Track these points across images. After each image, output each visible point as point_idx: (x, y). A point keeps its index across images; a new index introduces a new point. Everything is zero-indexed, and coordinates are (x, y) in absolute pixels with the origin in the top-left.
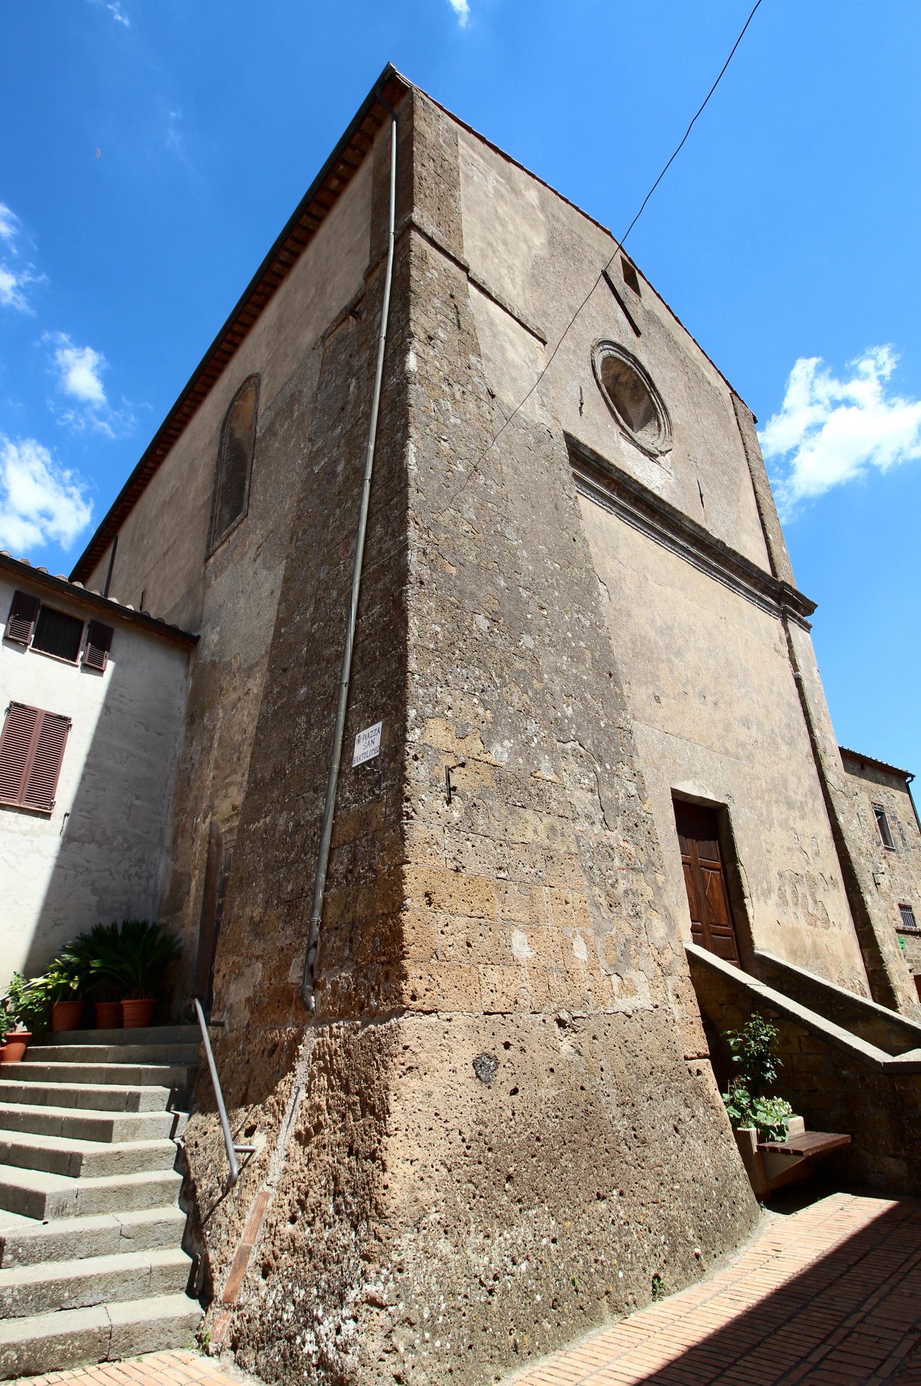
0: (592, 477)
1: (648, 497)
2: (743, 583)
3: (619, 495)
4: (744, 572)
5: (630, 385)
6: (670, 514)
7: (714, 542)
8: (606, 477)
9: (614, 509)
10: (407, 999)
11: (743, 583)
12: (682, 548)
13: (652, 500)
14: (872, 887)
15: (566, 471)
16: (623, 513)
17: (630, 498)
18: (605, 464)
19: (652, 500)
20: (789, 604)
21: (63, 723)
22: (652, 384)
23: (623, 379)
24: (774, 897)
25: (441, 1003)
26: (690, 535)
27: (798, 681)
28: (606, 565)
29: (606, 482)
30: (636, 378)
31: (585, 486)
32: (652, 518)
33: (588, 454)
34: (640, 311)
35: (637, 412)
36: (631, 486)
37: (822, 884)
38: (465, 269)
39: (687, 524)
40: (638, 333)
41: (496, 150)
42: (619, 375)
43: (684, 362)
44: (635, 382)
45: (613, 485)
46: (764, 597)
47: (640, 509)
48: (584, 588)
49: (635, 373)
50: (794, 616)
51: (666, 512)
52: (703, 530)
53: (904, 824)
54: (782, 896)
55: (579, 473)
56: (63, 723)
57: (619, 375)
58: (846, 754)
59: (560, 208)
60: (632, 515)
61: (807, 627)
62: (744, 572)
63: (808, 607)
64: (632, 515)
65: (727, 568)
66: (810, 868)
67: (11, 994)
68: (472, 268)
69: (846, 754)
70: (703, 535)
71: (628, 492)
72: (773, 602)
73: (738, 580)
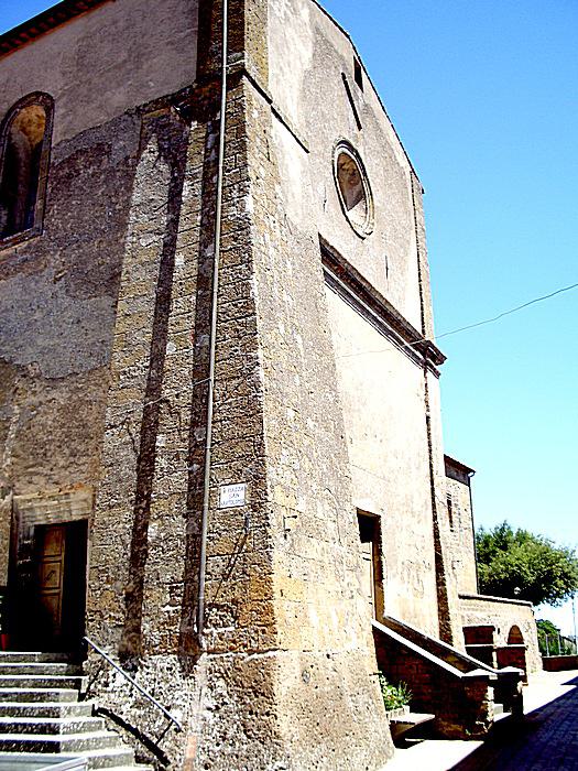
5: (351, 172)
7: (457, 665)
10: (277, 643)
14: (450, 571)
15: (318, 266)
20: (428, 356)
21: (75, 534)
22: (365, 174)
24: (399, 576)
25: (289, 647)
27: (431, 466)
28: (348, 379)
34: (361, 102)
35: (352, 194)
37: (423, 568)
38: (270, 101)
40: (360, 127)
43: (386, 146)
48: (328, 373)
50: (431, 366)
53: (462, 511)
54: (402, 579)
55: (326, 269)
56: (75, 534)
58: (447, 459)
59: (327, 23)
61: (437, 375)
63: (439, 358)
66: (418, 558)
68: (274, 98)
69: (447, 459)
72: (421, 357)
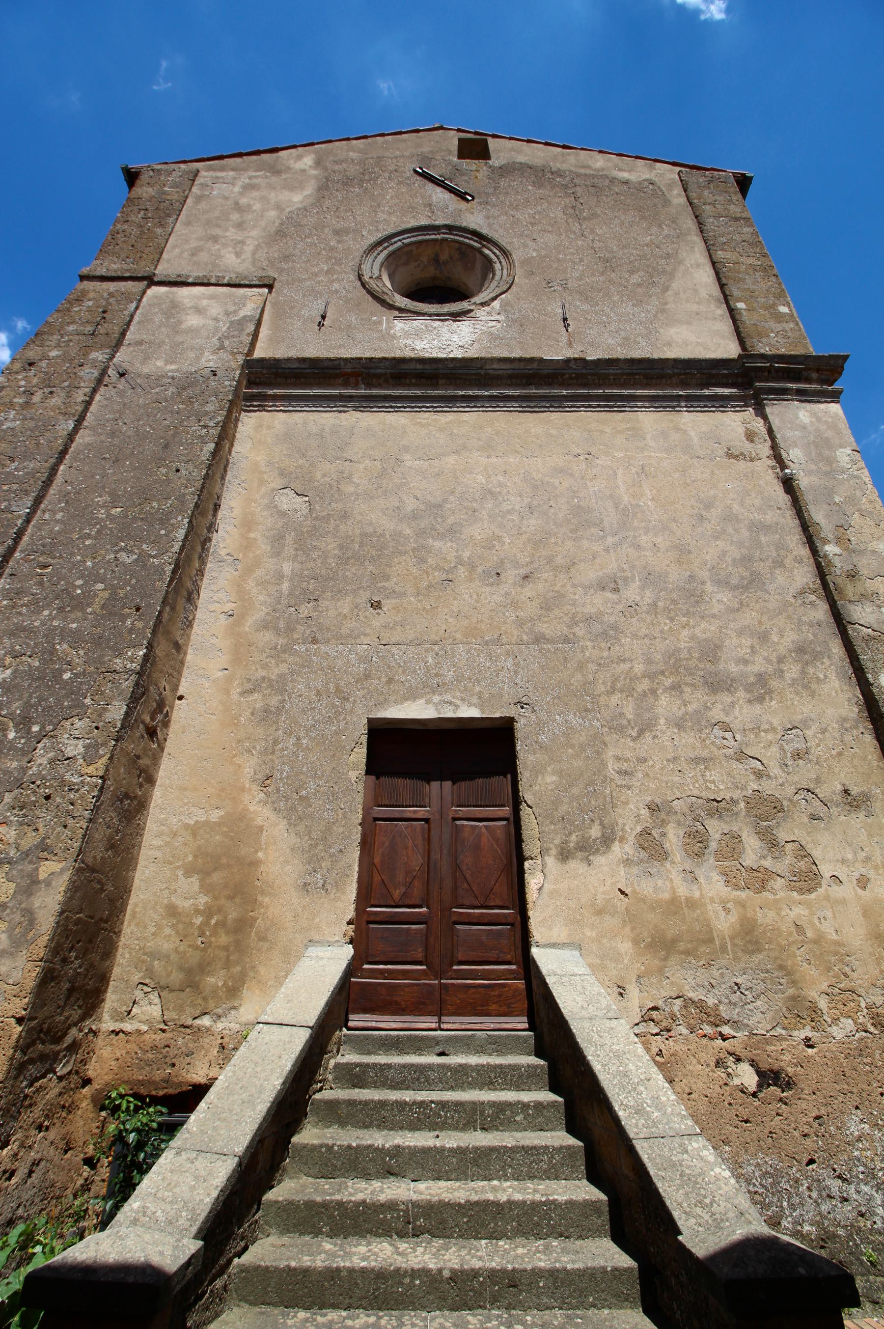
0: (319, 385)
1: (412, 366)
2: (639, 392)
3: (369, 386)
4: (647, 377)
6: (460, 368)
8: (337, 376)
9: (349, 404)
11: (639, 392)
12: (491, 398)
13: (419, 366)
16: (367, 403)
17: (386, 381)
18: (326, 364)
19: (419, 366)
23: (444, 257)
26: (510, 377)
29: (340, 381)
30: (457, 245)
31: (297, 401)
32: (435, 386)
33: (296, 365)
36: (377, 368)
39: (495, 366)
41: (257, 153)
42: (437, 255)
44: (459, 249)
45: (352, 380)
46: (706, 392)
47: (409, 386)
49: (453, 241)
51: (452, 369)
52: (532, 360)
57: (437, 255)
60: (386, 398)
62: (647, 377)
64: (386, 398)
65: (611, 386)
67: (136, 1225)
70: (535, 365)
71: (378, 376)
73: (626, 392)
